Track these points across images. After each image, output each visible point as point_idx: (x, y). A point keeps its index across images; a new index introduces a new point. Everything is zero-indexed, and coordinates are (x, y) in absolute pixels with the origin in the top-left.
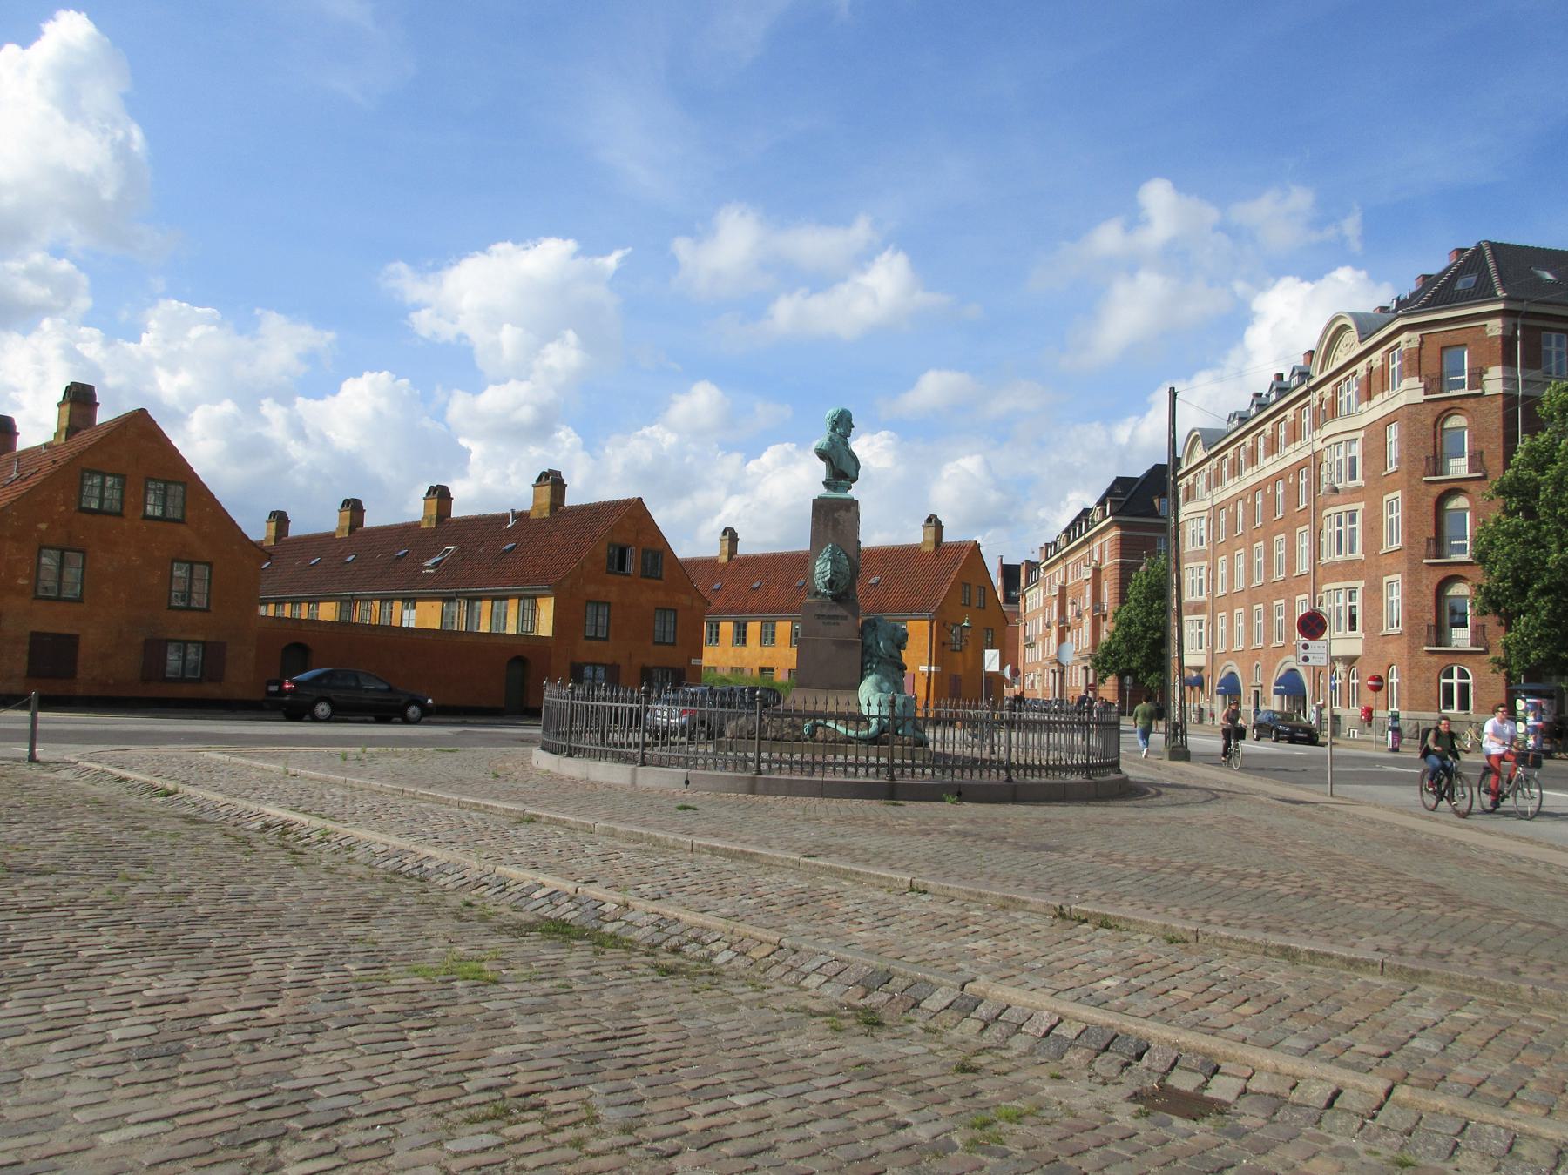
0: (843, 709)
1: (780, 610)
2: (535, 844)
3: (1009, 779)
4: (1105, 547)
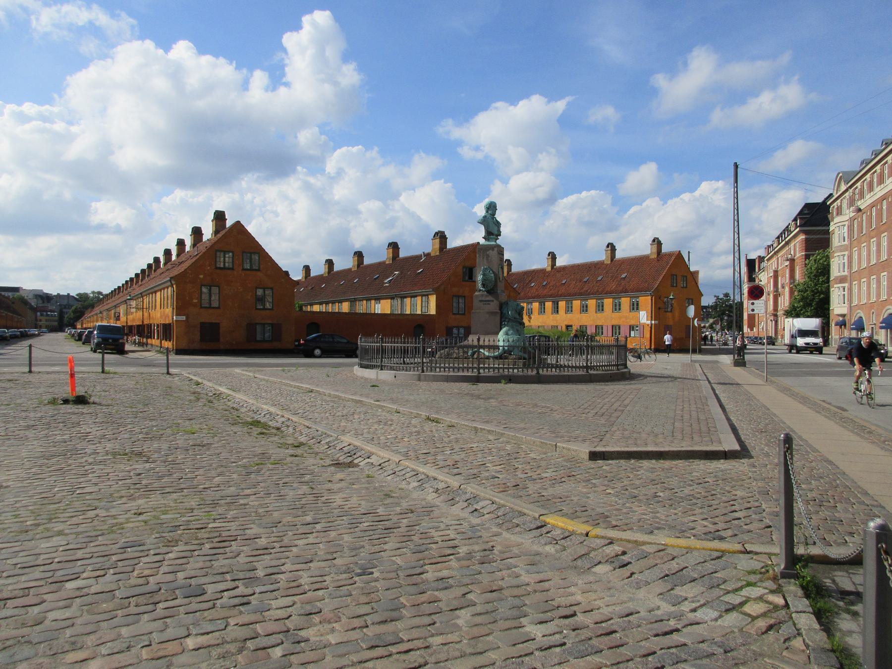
0: (492, 343)
1: (575, 294)
3: (538, 373)
4: (797, 248)
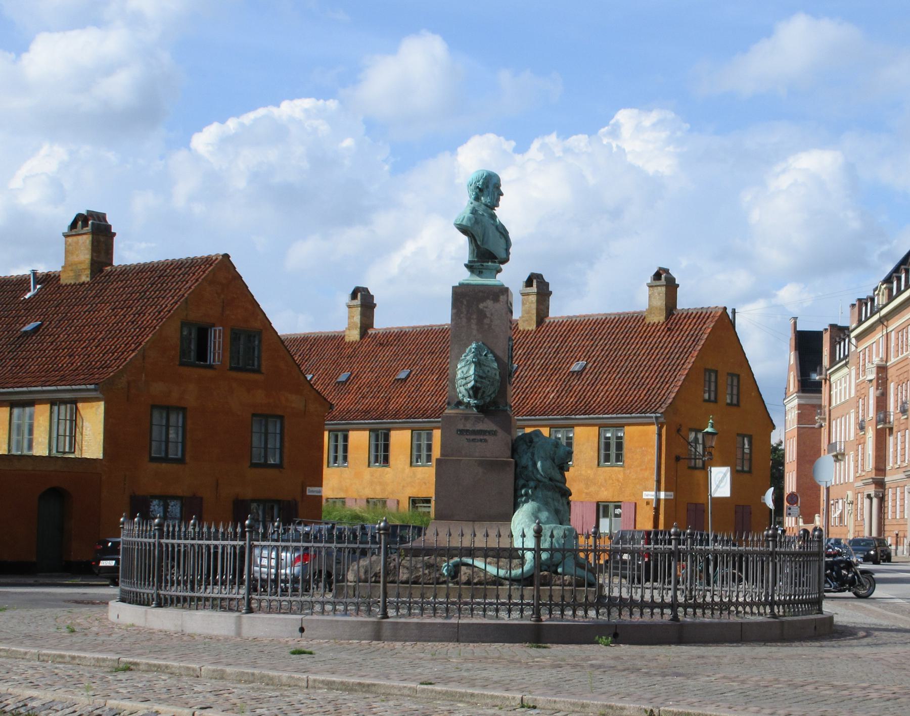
0: (493, 543)
2: (140, 685)
3: (675, 618)
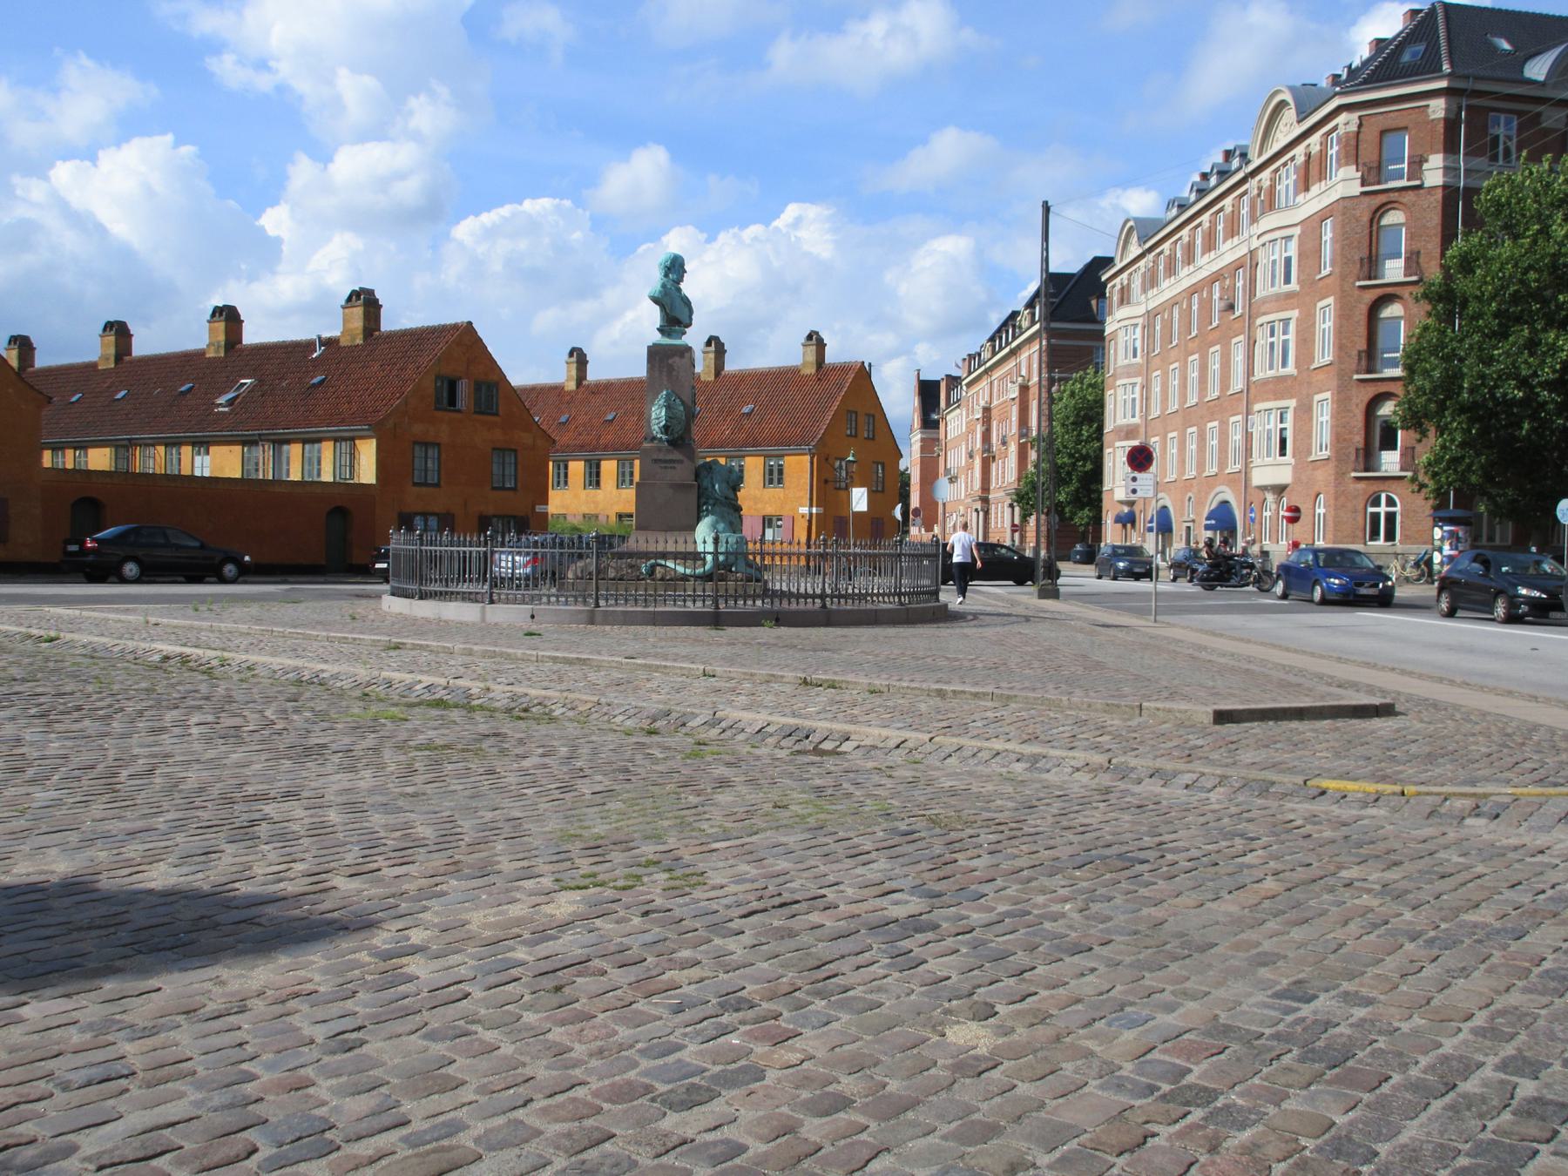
0: (681, 548)
3: (824, 606)
4: (1030, 361)
